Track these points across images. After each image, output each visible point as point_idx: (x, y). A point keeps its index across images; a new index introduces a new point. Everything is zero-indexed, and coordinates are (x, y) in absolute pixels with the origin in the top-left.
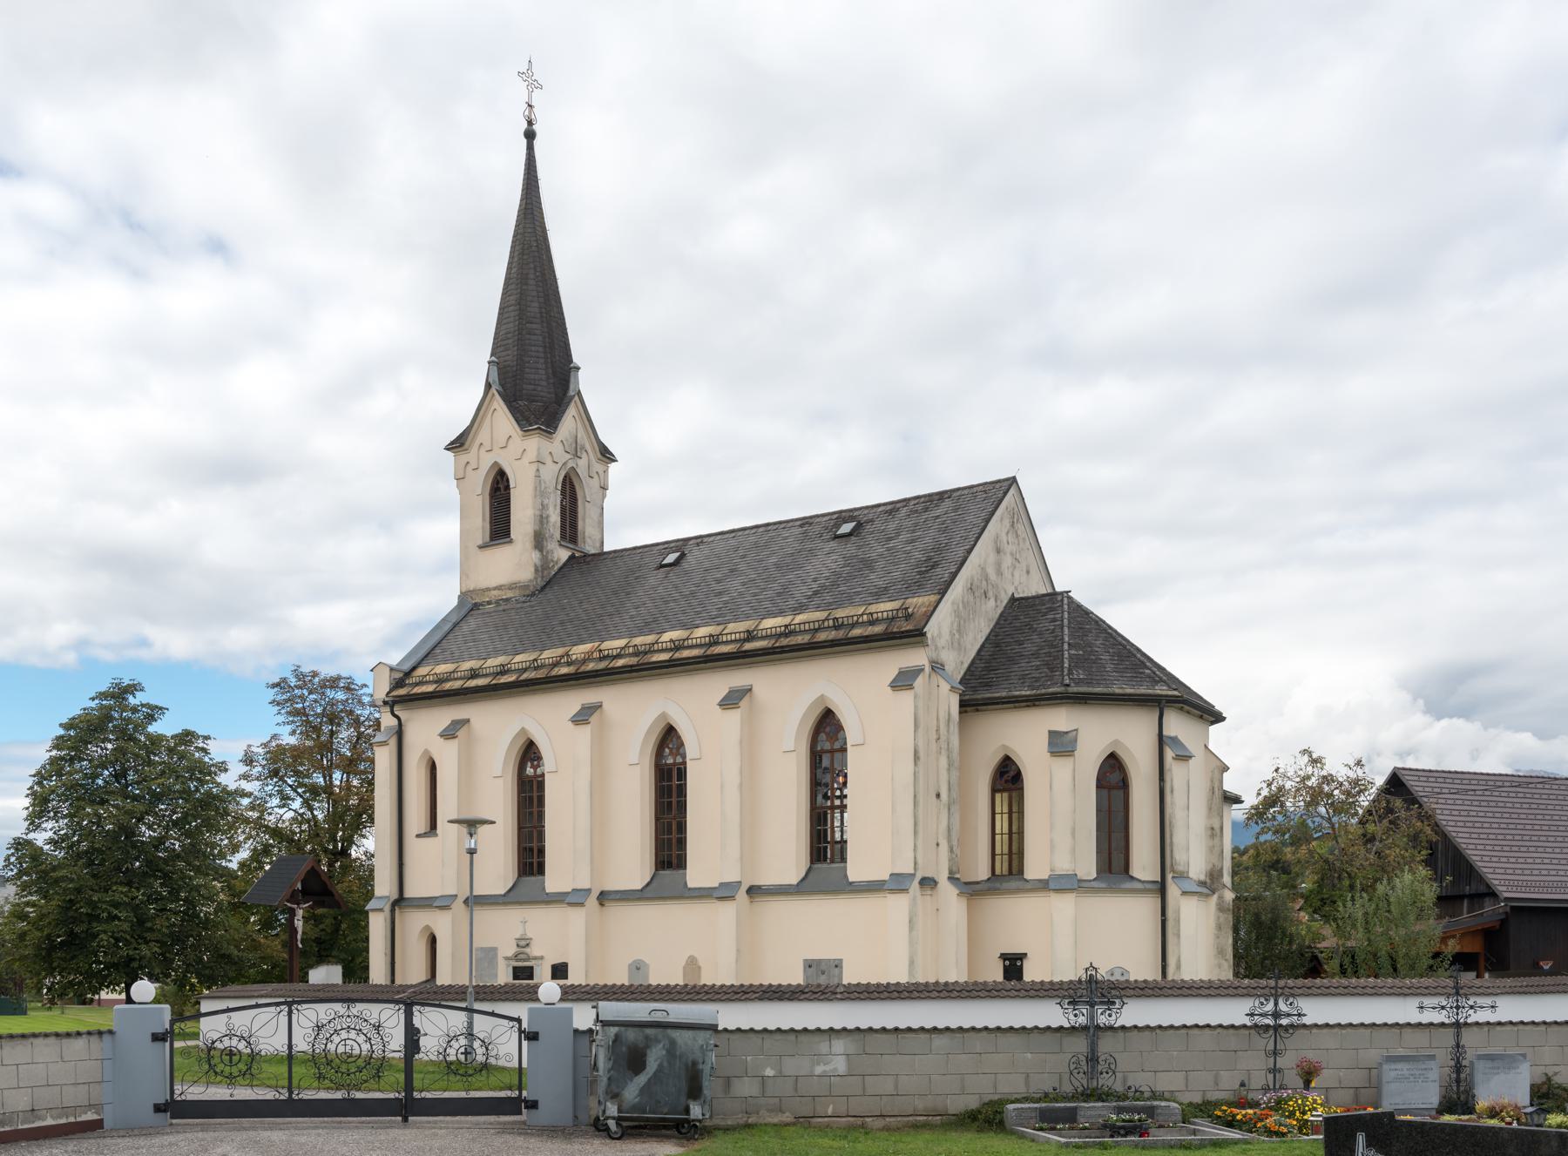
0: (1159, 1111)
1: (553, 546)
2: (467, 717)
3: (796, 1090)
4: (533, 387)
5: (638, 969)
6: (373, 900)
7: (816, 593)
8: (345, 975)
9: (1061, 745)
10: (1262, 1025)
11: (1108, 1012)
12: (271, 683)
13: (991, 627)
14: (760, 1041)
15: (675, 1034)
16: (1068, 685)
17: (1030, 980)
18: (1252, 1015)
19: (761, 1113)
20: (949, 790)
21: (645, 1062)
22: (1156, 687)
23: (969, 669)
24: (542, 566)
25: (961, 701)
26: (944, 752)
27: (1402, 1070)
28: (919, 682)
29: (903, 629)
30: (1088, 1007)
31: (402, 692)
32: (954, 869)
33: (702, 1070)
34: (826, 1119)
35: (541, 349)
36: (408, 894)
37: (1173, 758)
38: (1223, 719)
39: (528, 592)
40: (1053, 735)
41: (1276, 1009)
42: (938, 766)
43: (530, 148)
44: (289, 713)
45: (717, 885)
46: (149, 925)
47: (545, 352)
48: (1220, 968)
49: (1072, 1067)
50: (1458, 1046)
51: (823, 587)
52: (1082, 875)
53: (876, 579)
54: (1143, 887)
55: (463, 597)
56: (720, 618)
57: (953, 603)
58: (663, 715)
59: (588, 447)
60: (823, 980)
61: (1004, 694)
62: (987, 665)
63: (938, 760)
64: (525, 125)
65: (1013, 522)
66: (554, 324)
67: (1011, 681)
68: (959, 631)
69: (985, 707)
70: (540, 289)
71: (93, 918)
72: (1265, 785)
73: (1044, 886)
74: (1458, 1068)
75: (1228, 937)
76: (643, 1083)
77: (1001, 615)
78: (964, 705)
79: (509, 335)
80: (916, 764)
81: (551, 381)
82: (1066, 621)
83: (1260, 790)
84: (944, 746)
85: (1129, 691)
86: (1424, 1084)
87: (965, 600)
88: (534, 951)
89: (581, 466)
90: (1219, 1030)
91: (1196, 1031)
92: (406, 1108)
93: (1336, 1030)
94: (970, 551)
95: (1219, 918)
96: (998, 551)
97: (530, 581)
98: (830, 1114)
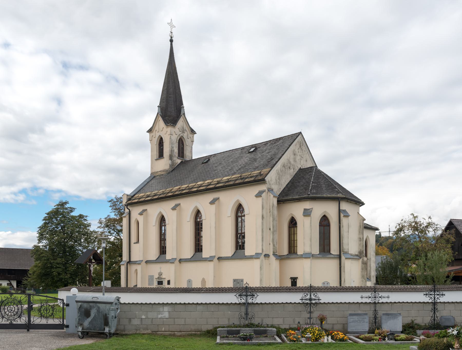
0: (268, 331)
1: (175, 159)
2: (146, 209)
3: (152, 323)
4: (170, 113)
5: (189, 282)
6: (122, 262)
7: (239, 169)
8: (112, 284)
9: (307, 213)
10: (305, 303)
11: (252, 298)
12: (109, 201)
13: (292, 178)
14: (140, 307)
15: (100, 305)
16: (309, 195)
17: (298, 286)
18: (302, 299)
19: (141, 330)
20: (273, 227)
21: (90, 314)
22: (338, 195)
23: (283, 190)
24: (172, 164)
25: (277, 200)
26: (272, 216)
27: (355, 318)
28: (264, 195)
29: (259, 179)
30: (245, 297)
31: (130, 202)
32: (275, 251)
33: (108, 317)
34: (162, 332)
35: (173, 102)
36: (132, 260)
37: (343, 216)
38: (364, 204)
39: (168, 172)
40: (305, 210)
41: (311, 297)
42: (270, 220)
43: (171, 45)
44: (115, 209)
45: (209, 257)
46: (68, 269)
47: (174, 103)
48: (363, 281)
49: (240, 316)
50: (375, 310)
51: (242, 167)
52: (313, 253)
53: (256, 164)
54: (334, 257)
55: (152, 174)
56: (212, 178)
57: (277, 171)
58: (238, 200)
59: (187, 130)
60: (238, 286)
61: (291, 198)
62: (288, 189)
63: (270, 218)
64: (170, 38)
65: (301, 146)
66: (177, 95)
67: (294, 194)
68: (279, 179)
69: (286, 202)
70: (173, 85)
71: (52, 267)
72: (398, 225)
73: (301, 257)
74: (375, 318)
75: (365, 272)
76: (90, 321)
77: (296, 174)
78: (279, 202)
79: (164, 99)
80: (262, 220)
81: (176, 111)
82: (313, 175)
83: (396, 226)
84: (272, 214)
85: (329, 196)
86: (363, 323)
87: (282, 169)
88: (163, 276)
89: (185, 135)
90: (295, 304)
91: (287, 305)
92: (28, 326)
93: (336, 305)
94: (283, 155)
95: (362, 266)
96: (295, 154)
97: (169, 169)
98: (163, 331)
